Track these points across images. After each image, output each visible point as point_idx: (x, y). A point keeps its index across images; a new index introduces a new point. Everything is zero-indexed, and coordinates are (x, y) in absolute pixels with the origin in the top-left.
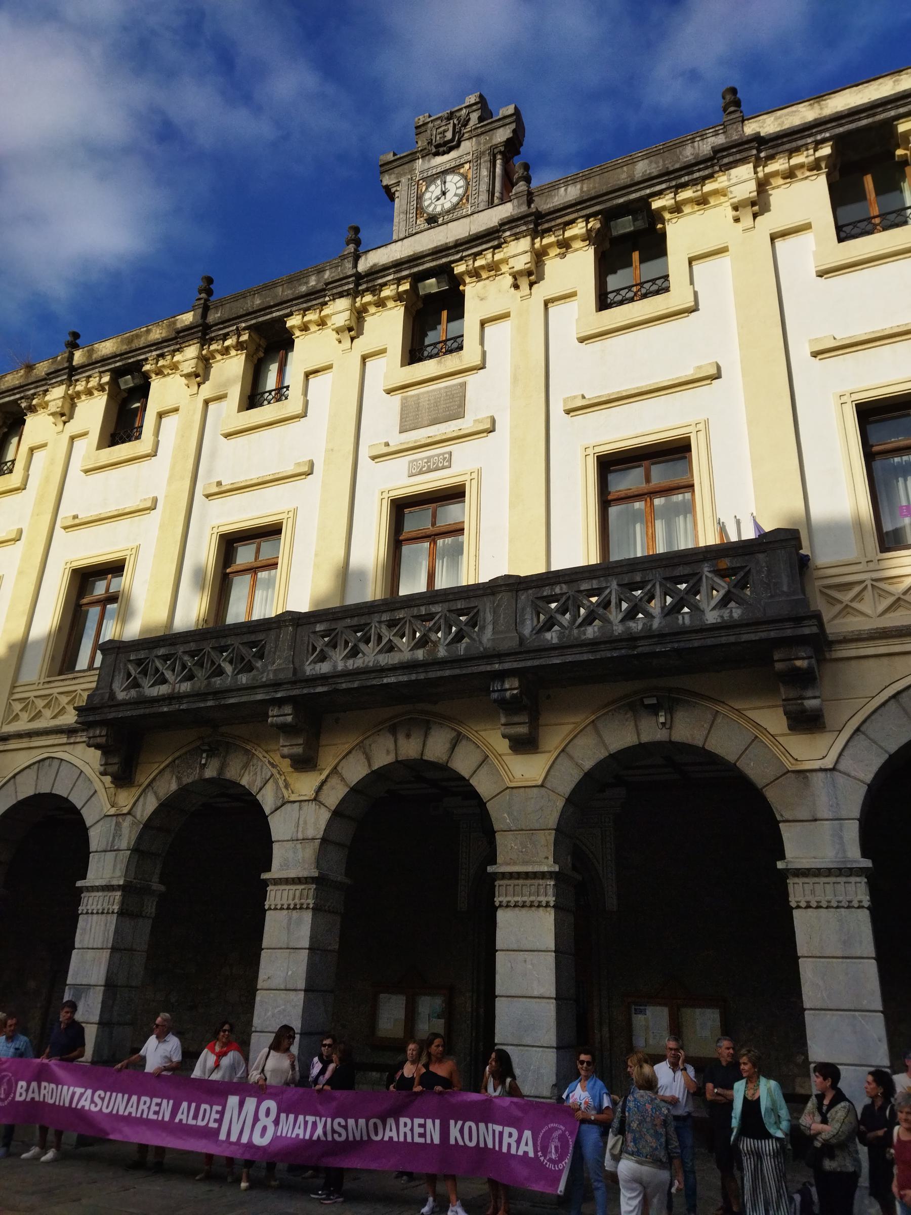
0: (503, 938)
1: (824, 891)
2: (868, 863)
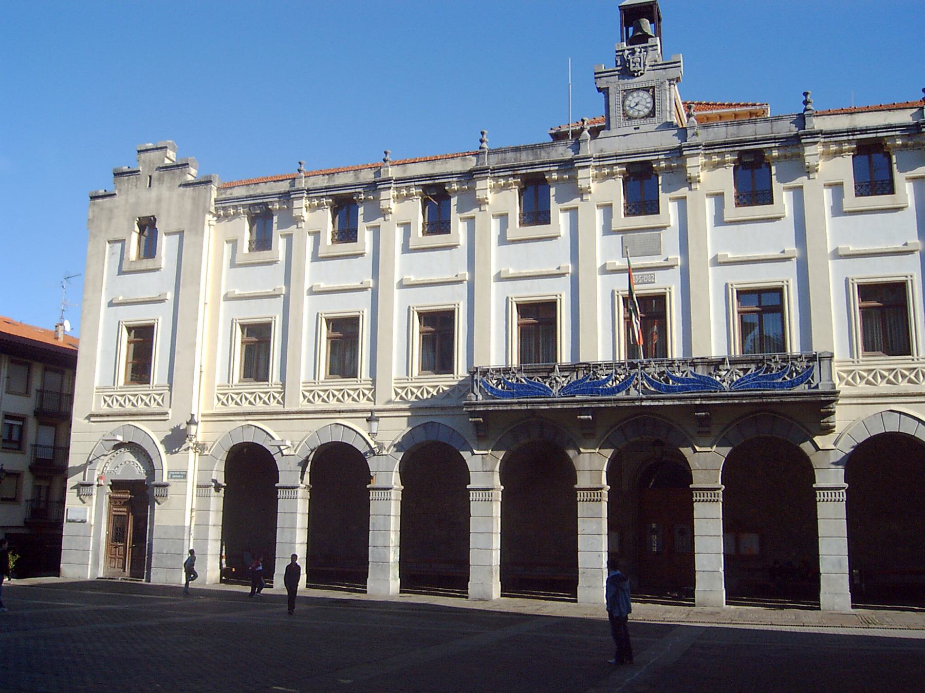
0: (696, 514)
1: (708, 495)
2: (847, 485)
